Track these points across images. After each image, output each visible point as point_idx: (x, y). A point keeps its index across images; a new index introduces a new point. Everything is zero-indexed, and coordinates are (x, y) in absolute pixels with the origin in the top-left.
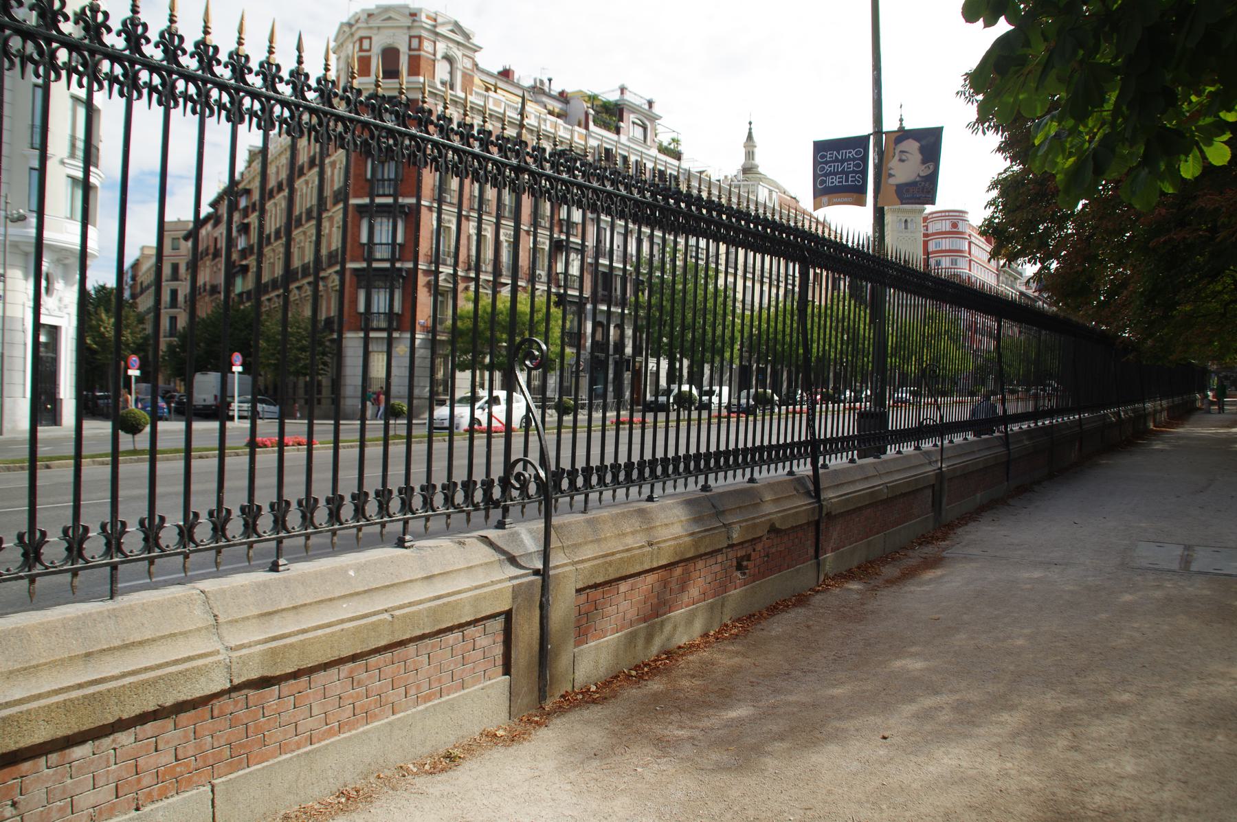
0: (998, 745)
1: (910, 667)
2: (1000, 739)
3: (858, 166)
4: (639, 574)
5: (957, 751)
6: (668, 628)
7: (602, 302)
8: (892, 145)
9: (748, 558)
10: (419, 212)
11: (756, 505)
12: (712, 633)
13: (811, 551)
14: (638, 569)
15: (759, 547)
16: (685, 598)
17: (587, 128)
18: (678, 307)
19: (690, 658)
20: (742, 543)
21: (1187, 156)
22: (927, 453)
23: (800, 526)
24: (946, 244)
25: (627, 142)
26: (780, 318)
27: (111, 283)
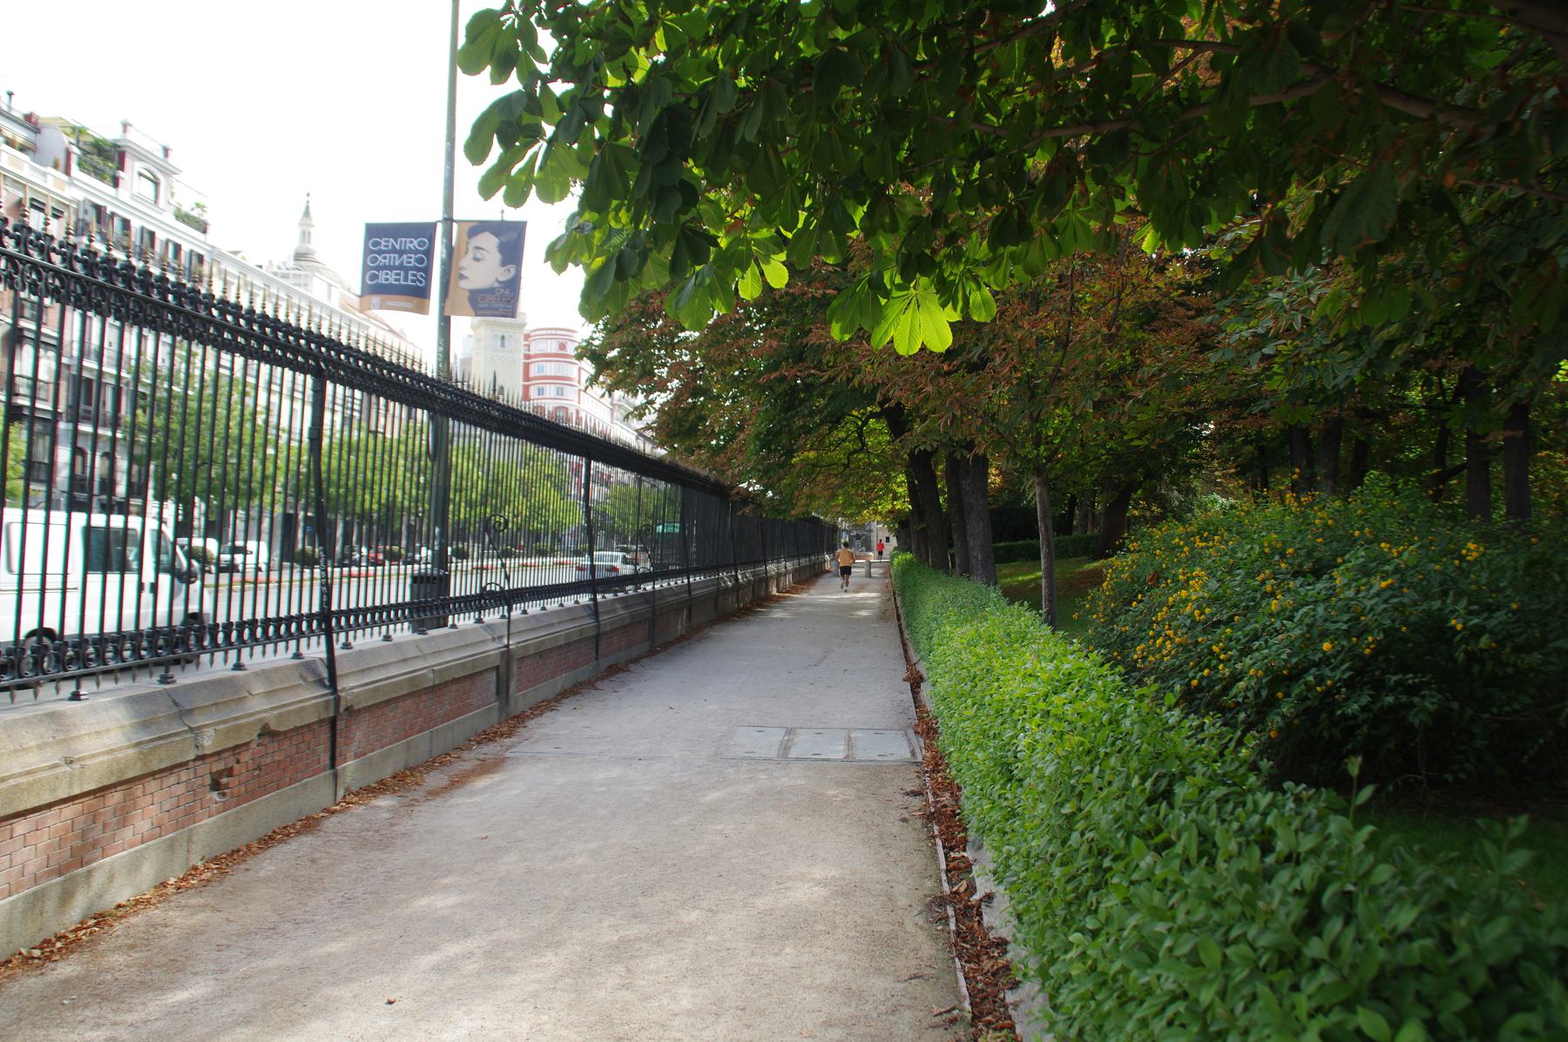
0: (535, 995)
1: (440, 904)
2: (538, 987)
3: (421, 261)
4: (50, 806)
5: (481, 1009)
6: (98, 880)
7: (86, 419)
8: (465, 238)
9: (229, 772)
11: (241, 700)
12: (172, 881)
13: (325, 759)
14: (47, 798)
15: (246, 757)
16: (127, 833)
17: (67, 172)
18: (190, 430)
19: (133, 920)
20: (218, 753)
21: (744, 270)
22: (490, 627)
23: (309, 726)
24: (551, 369)
25: (130, 198)
26: (336, 453)
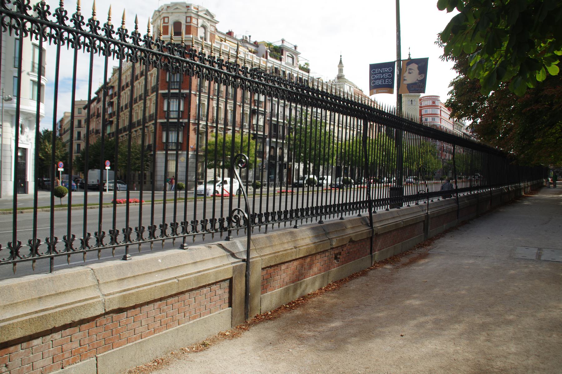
0: (454, 339)
1: (414, 303)
2: (454, 336)
3: (390, 75)
4: (290, 261)
5: (435, 342)
6: (303, 286)
7: (274, 137)
8: (405, 66)
9: (340, 254)
10: (190, 97)
11: (344, 230)
12: (323, 288)
13: (369, 251)
14: (290, 259)
15: (345, 249)
16: (311, 272)
17: (267, 58)
18: (308, 140)
19: (314, 299)
20: (337, 247)
21: (539, 71)
22: (421, 206)
23: (364, 239)
24: (430, 111)
25: (285, 65)
26: (355, 145)
27: (51, 129)
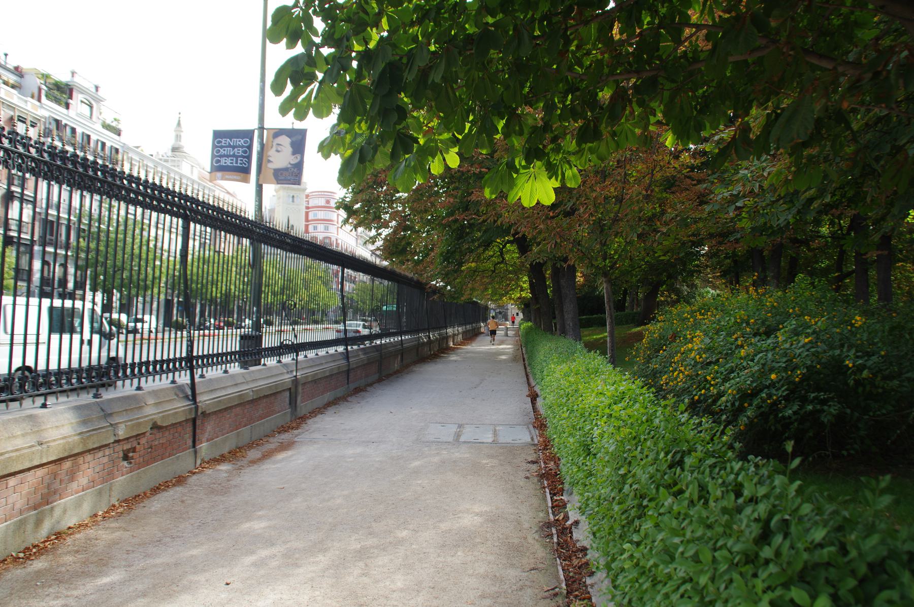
0: (312, 579)
1: (256, 527)
2: (314, 575)
3: (245, 152)
4: (29, 469)
5: (280, 588)
6: (57, 513)
7: (50, 244)
8: (271, 139)
9: (134, 450)
11: (141, 408)
12: (100, 513)
13: (190, 442)
14: (27, 465)
15: (143, 441)
16: (74, 485)
17: (39, 100)
18: (111, 250)
19: (77, 536)
20: (127, 439)
21: (434, 157)
22: (286, 365)
23: (180, 423)
24: (321, 215)
25: (76, 115)
26: (196, 264)
